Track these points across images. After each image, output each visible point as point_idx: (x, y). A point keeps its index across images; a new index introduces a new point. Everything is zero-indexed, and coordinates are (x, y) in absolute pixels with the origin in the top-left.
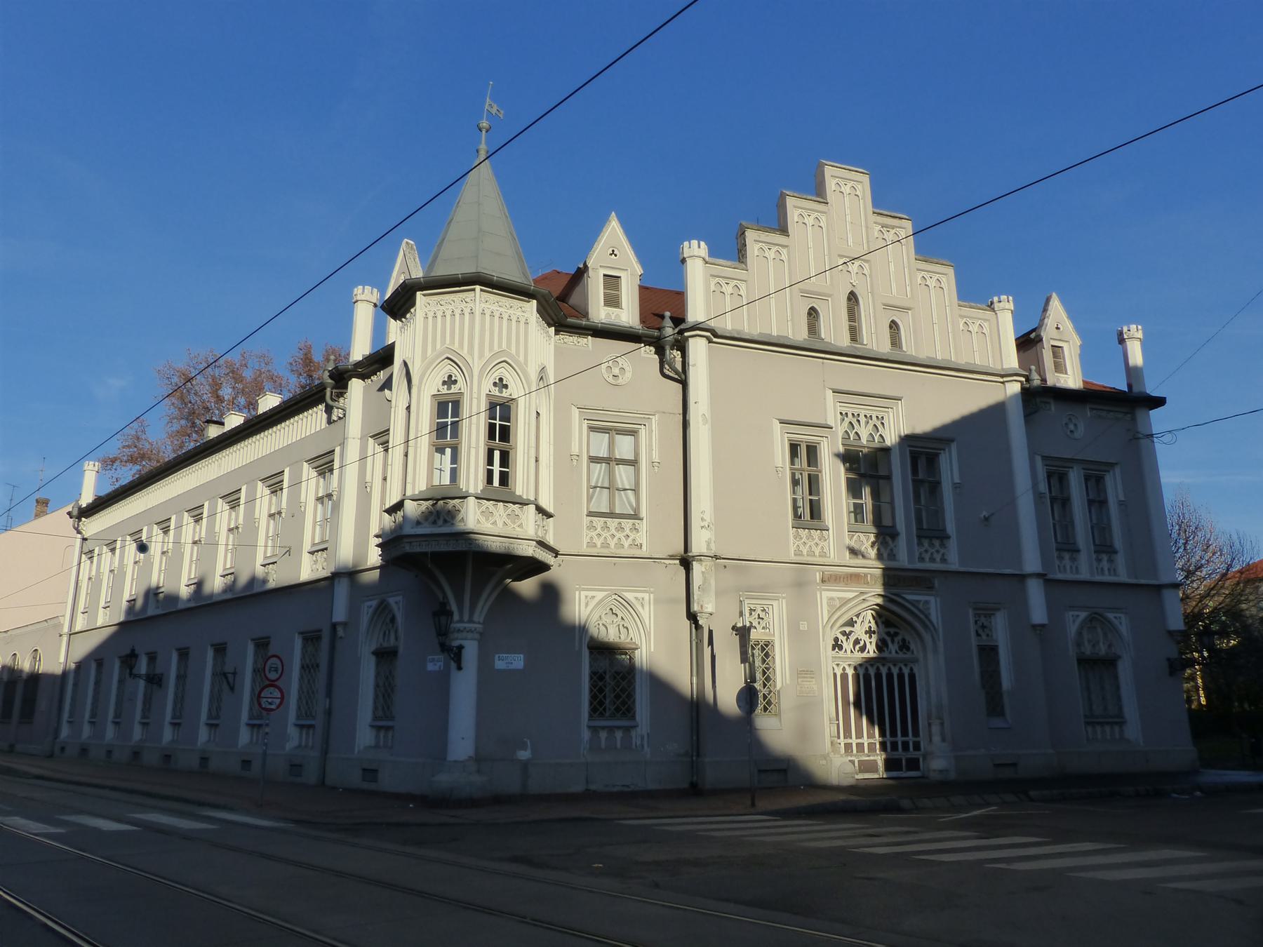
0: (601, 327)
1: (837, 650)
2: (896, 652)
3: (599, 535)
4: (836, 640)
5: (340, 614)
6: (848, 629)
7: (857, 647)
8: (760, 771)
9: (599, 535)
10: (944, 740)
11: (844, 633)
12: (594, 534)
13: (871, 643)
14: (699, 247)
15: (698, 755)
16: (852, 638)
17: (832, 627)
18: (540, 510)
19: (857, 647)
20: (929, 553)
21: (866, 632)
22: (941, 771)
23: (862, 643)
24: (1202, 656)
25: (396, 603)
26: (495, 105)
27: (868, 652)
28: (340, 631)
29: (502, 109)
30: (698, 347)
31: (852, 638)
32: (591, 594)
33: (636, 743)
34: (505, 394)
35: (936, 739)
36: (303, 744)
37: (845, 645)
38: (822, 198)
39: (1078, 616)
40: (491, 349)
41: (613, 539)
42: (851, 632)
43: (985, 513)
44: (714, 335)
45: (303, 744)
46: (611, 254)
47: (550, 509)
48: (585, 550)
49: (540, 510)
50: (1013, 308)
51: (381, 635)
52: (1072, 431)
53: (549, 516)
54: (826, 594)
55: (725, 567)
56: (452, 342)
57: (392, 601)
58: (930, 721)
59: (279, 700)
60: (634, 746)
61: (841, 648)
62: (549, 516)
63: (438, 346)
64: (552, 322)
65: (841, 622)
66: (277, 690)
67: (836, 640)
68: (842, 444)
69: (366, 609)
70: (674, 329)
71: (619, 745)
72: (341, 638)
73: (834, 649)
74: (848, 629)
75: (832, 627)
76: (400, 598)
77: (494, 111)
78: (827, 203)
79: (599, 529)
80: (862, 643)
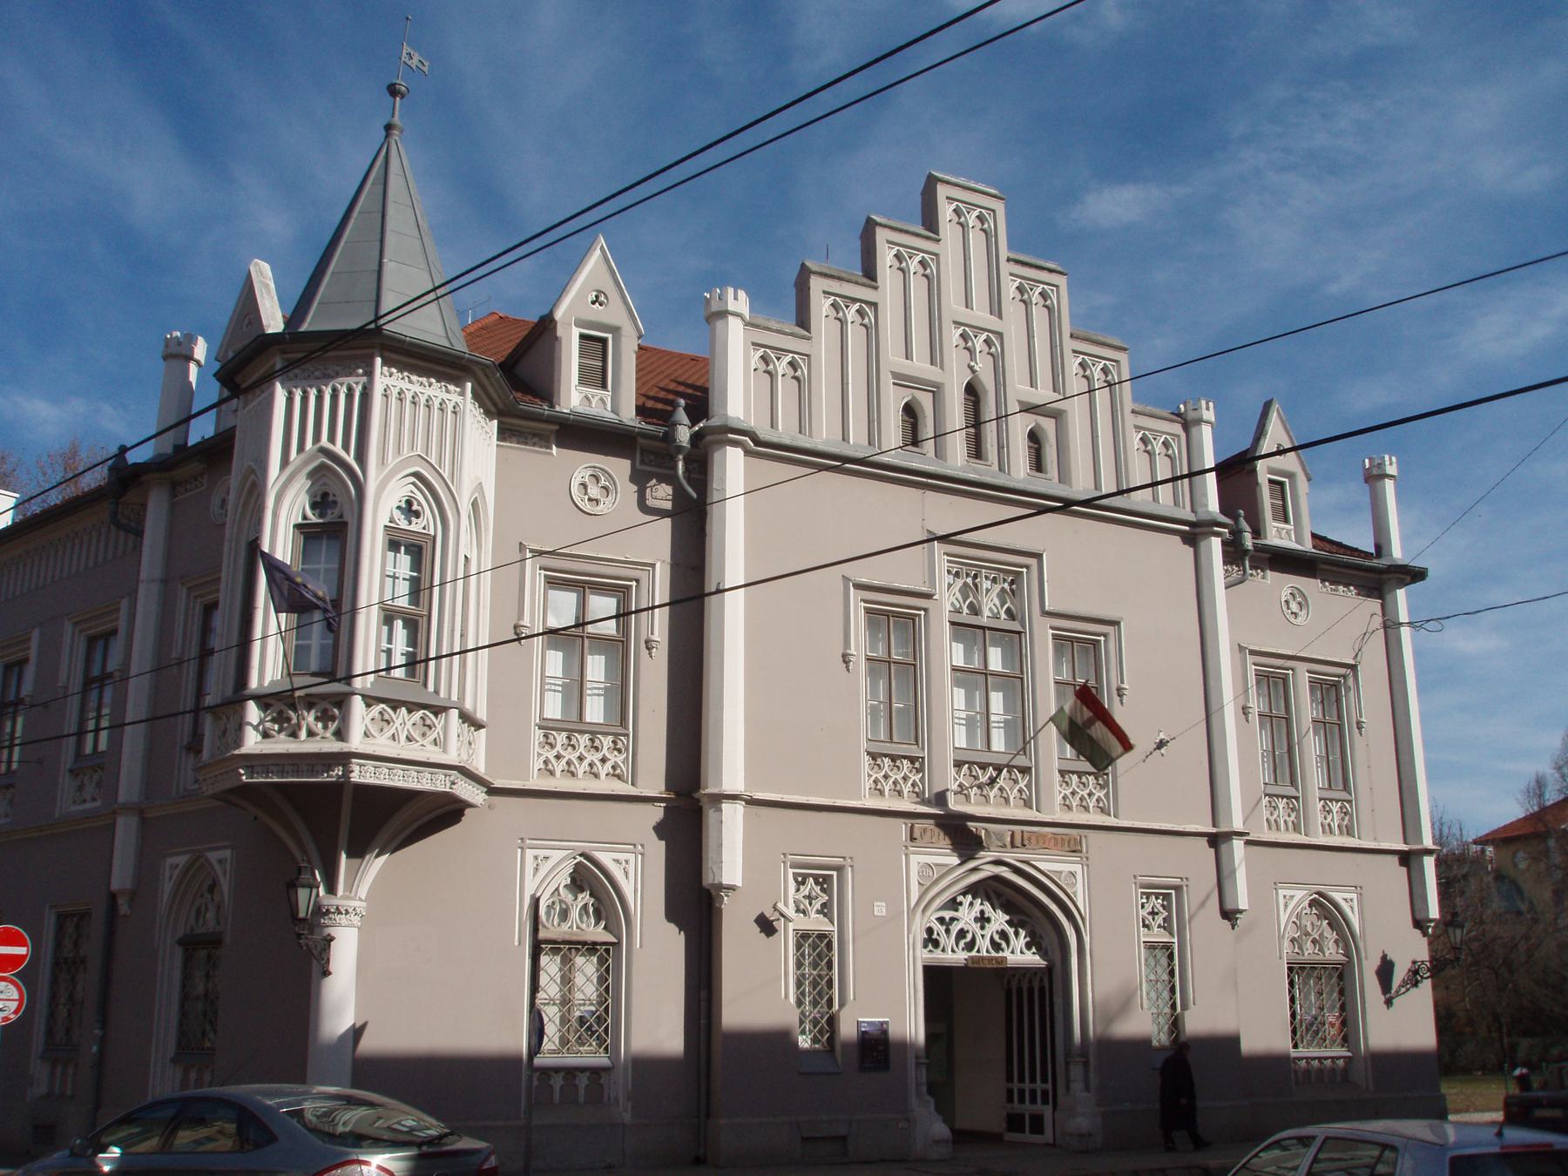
0: (574, 420)
1: (930, 947)
2: (1022, 952)
3: (558, 757)
4: (930, 931)
5: (121, 877)
6: (947, 915)
7: (962, 944)
8: (805, 1140)
9: (558, 757)
10: (1087, 1089)
11: (941, 920)
12: (551, 755)
13: (983, 936)
14: (736, 298)
15: (708, 1115)
16: (955, 928)
17: (924, 911)
18: (466, 718)
19: (962, 944)
20: (564, 761)
21: (976, 920)
22: (1081, 1136)
23: (969, 937)
24: (1475, 971)
25: (220, 861)
26: (416, 55)
27: (978, 951)
28: (123, 908)
29: (427, 61)
30: (733, 466)
31: (955, 928)
32: (542, 853)
33: (609, 1095)
34: (417, 525)
35: (1077, 1086)
36: (57, 1091)
37: (943, 940)
38: (933, 233)
39: (1292, 897)
40: (399, 451)
41: (580, 764)
42: (953, 919)
43: (1162, 736)
44: (761, 448)
45: (57, 1091)
46: (593, 303)
47: (482, 715)
48: (536, 782)
49: (466, 718)
50: (1213, 420)
51: (193, 914)
52: (1295, 614)
53: (478, 726)
54: (916, 860)
55: (256, 818)
56: (332, 439)
57: (213, 856)
58: (1069, 1060)
59: (17, 1003)
60: (605, 1100)
61: (936, 944)
62: (478, 726)
63: (309, 444)
64: (493, 409)
65: (938, 902)
66: (11, 986)
67: (930, 931)
68: (952, 623)
69: (167, 868)
70: (690, 428)
71: (581, 1099)
72: (125, 916)
73: (925, 946)
74: (947, 915)
75: (924, 911)
76: (227, 853)
77: (414, 63)
78: (938, 241)
79: (582, 749)
80: (969, 937)
